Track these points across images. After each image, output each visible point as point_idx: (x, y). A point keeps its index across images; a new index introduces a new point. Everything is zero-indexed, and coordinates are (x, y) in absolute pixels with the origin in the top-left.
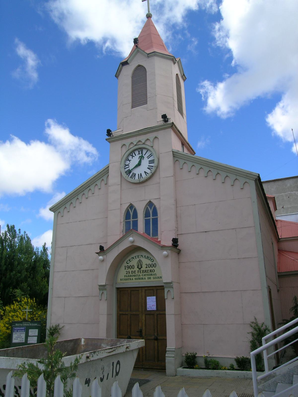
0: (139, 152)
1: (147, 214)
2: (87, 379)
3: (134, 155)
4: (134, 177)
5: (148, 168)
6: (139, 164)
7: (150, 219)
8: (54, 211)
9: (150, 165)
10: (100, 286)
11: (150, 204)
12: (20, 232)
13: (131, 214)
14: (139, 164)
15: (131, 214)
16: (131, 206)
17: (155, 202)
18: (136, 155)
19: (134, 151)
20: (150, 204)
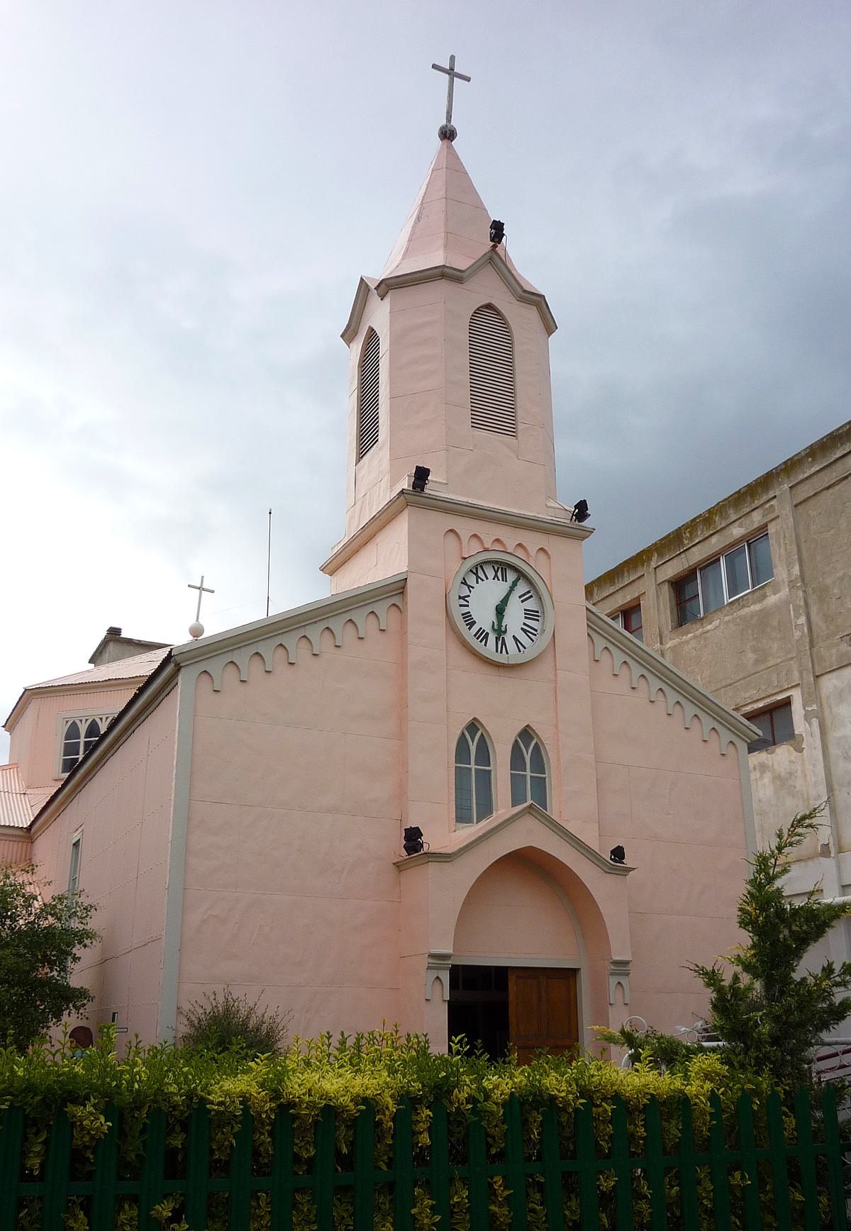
0: (496, 572)
1: (517, 759)
2: (73, 732)
3: (481, 574)
4: (529, 634)
5: (522, 629)
6: (500, 611)
7: (79, 742)
8: (555, 328)
9: (529, 622)
10: (432, 956)
11: (527, 734)
12: (698, 967)
13: (473, 749)
14: (500, 611)
15: (473, 749)
16: (473, 726)
17: (544, 733)
18: (487, 579)
19: (481, 565)
20: (527, 734)
